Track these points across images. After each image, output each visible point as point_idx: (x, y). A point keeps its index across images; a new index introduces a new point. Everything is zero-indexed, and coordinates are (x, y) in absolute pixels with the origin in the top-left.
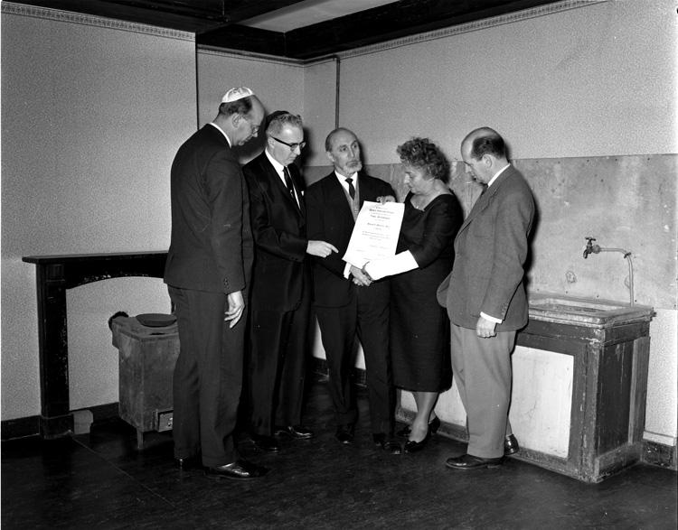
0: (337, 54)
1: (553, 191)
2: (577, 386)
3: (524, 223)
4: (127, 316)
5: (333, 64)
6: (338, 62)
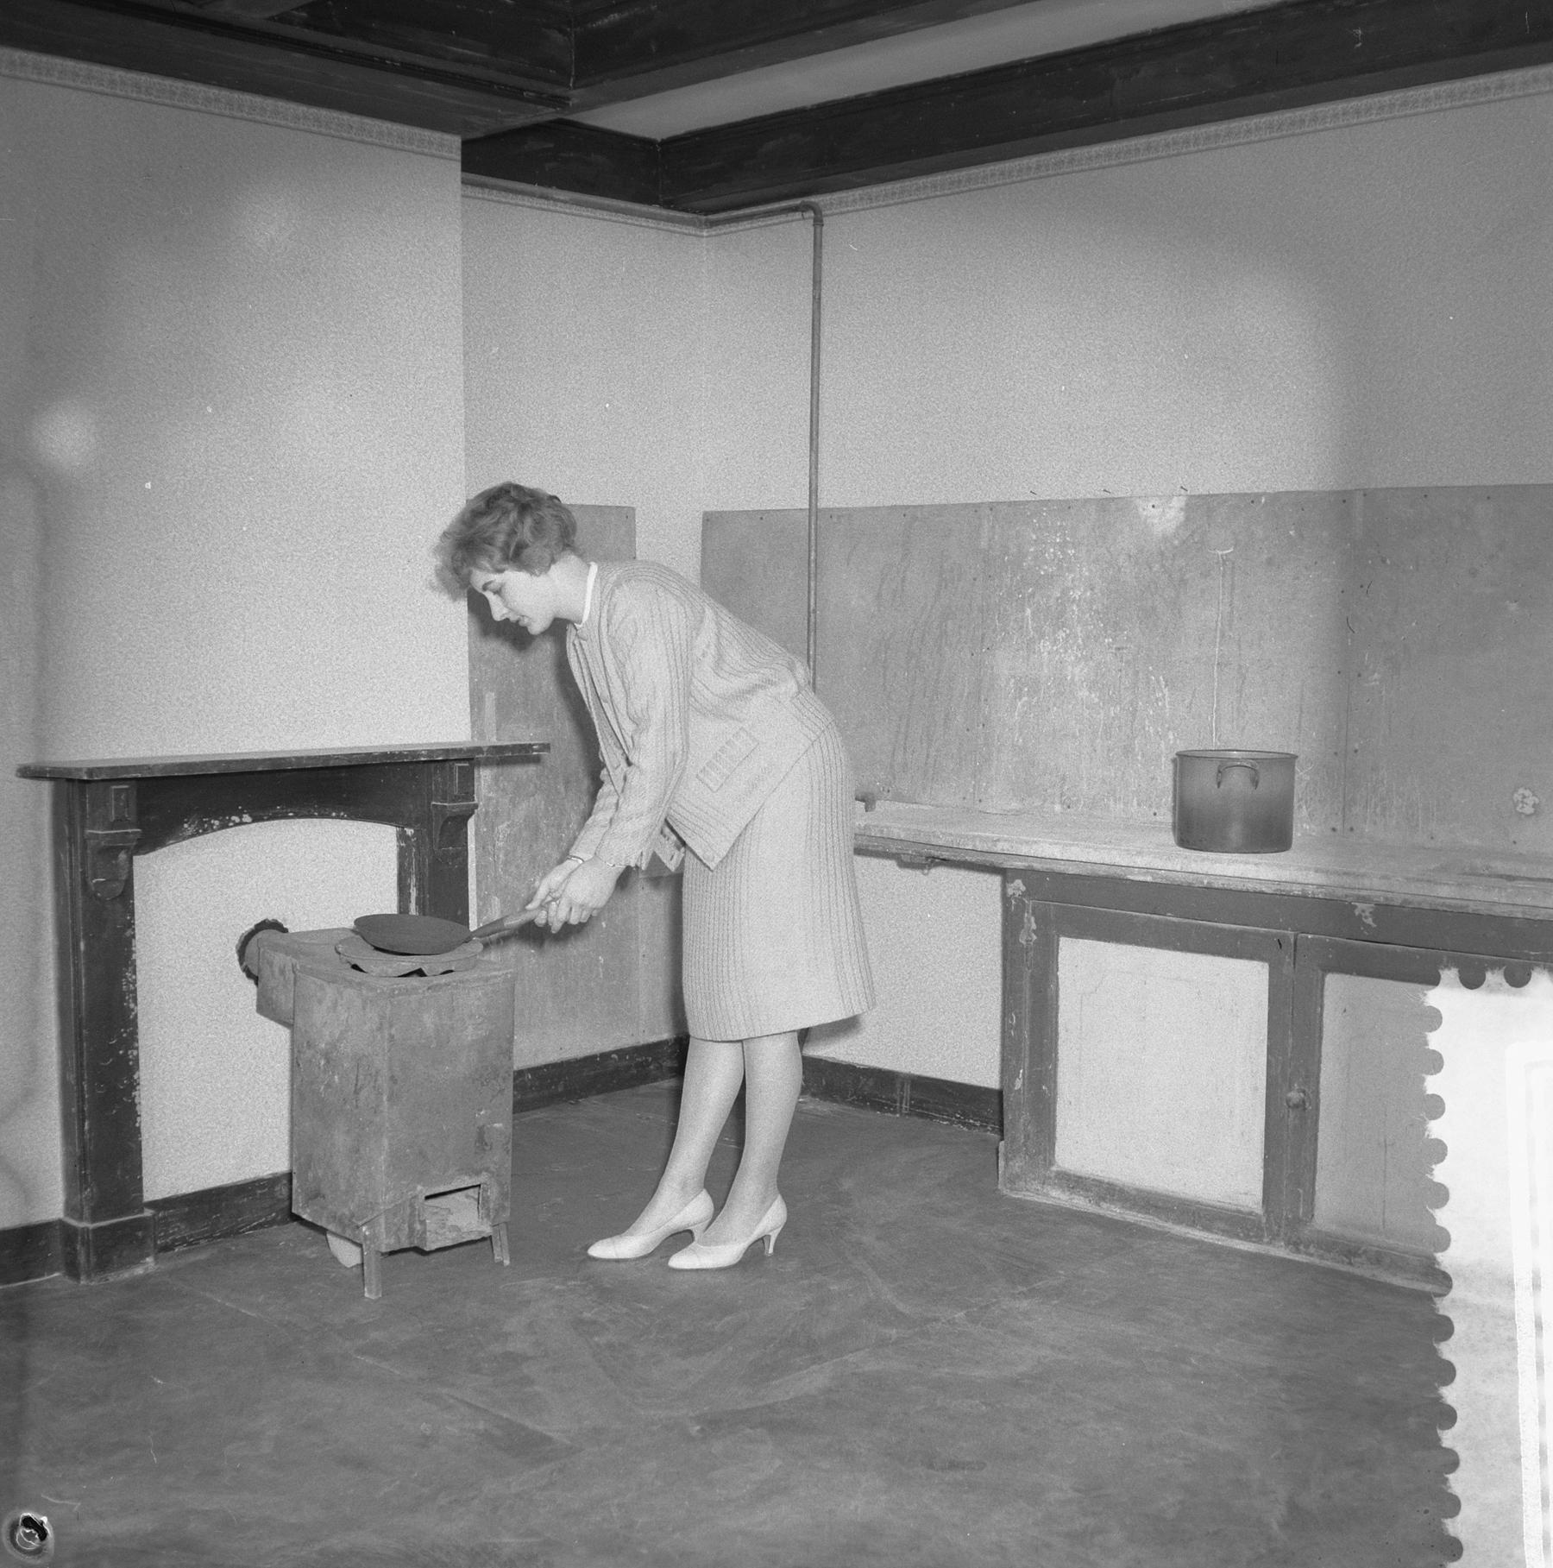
0: (813, 199)
1: (1473, 573)
2: (1317, 1046)
3: (571, 505)
4: (285, 931)
5: (798, 229)
6: (818, 222)
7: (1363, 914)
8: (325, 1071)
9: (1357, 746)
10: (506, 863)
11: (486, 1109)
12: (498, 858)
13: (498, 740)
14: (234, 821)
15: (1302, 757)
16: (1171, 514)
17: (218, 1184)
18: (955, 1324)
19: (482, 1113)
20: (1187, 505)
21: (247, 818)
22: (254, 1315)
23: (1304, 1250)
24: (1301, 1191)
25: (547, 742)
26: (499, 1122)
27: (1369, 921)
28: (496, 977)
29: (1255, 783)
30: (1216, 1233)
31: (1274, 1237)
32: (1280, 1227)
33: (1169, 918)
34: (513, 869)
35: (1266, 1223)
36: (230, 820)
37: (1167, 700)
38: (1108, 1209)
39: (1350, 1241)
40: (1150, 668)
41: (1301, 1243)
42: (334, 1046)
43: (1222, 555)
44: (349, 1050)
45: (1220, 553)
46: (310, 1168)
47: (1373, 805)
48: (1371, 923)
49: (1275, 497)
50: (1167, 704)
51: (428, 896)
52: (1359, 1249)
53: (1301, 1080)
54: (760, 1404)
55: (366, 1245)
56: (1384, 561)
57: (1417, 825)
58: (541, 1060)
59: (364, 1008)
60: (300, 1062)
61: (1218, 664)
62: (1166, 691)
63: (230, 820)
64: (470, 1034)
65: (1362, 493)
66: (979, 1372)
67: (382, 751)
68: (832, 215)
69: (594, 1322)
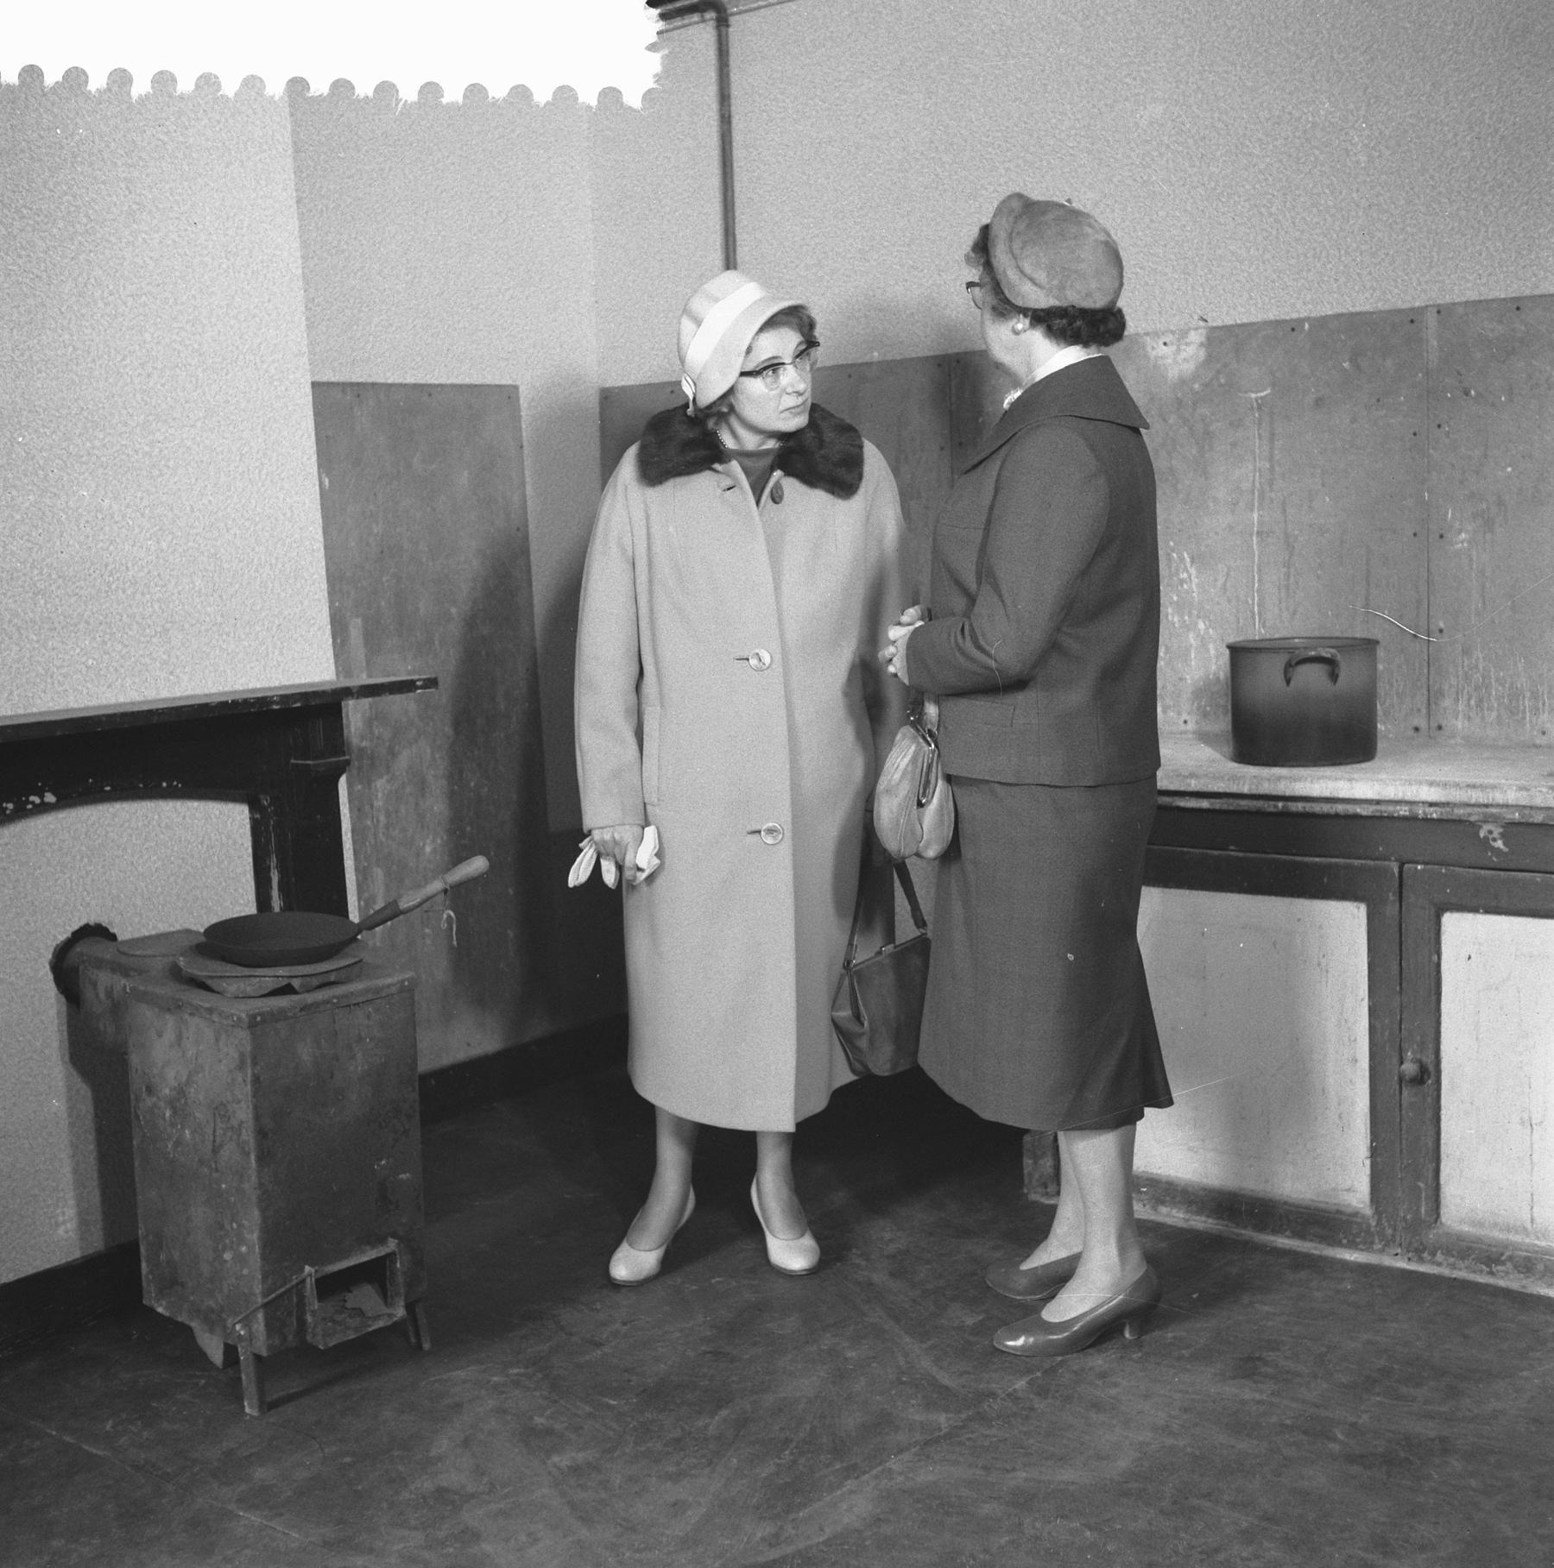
4: (113, 937)
7: (1490, 837)
8: (173, 1125)
9: (1442, 625)
10: (387, 827)
11: (388, 1158)
12: (378, 821)
13: (369, 676)
14: (33, 803)
15: (1383, 643)
16: (1190, 351)
17: (48, 1266)
18: (1017, 1399)
19: (383, 1162)
20: (1208, 338)
21: (50, 798)
22: (100, 1453)
23: (1429, 1258)
24: (1421, 1185)
25: (433, 676)
26: (405, 1173)
27: (1499, 844)
28: (389, 986)
29: (1334, 677)
30: (1311, 1240)
31: (1388, 1243)
32: (1395, 1230)
33: (1232, 853)
34: (395, 833)
35: (1376, 1226)
36: (27, 802)
37: (1195, 580)
38: (1168, 1215)
39: (1489, 1245)
40: (1172, 544)
41: (1425, 1248)
42: (181, 1092)
43: (1256, 400)
44: (201, 1097)
45: (1253, 396)
46: (161, 1248)
47: (1466, 697)
48: (1502, 847)
49: (1321, 323)
50: (1194, 586)
51: (293, 879)
52: (1502, 1254)
53: (1415, 1047)
54: (790, 1549)
55: (243, 1348)
56: (1467, 393)
57: (1524, 718)
58: (447, 1060)
59: (217, 1040)
60: (139, 1112)
61: (1258, 532)
62: (1193, 571)
63: (27, 802)
64: (358, 1065)
65: (1435, 310)
66: (1067, 1475)
67: (219, 700)
68: (740, 13)
69: (549, 1432)
